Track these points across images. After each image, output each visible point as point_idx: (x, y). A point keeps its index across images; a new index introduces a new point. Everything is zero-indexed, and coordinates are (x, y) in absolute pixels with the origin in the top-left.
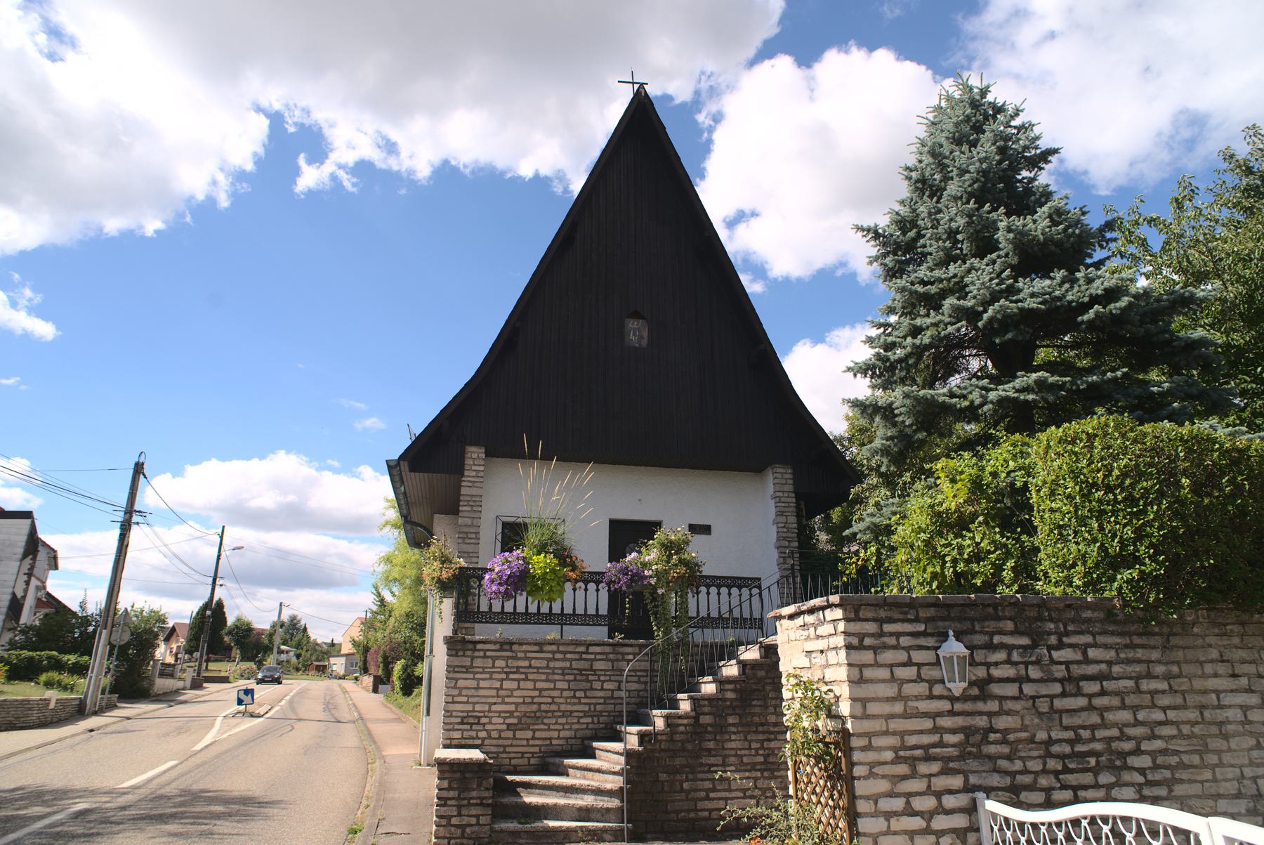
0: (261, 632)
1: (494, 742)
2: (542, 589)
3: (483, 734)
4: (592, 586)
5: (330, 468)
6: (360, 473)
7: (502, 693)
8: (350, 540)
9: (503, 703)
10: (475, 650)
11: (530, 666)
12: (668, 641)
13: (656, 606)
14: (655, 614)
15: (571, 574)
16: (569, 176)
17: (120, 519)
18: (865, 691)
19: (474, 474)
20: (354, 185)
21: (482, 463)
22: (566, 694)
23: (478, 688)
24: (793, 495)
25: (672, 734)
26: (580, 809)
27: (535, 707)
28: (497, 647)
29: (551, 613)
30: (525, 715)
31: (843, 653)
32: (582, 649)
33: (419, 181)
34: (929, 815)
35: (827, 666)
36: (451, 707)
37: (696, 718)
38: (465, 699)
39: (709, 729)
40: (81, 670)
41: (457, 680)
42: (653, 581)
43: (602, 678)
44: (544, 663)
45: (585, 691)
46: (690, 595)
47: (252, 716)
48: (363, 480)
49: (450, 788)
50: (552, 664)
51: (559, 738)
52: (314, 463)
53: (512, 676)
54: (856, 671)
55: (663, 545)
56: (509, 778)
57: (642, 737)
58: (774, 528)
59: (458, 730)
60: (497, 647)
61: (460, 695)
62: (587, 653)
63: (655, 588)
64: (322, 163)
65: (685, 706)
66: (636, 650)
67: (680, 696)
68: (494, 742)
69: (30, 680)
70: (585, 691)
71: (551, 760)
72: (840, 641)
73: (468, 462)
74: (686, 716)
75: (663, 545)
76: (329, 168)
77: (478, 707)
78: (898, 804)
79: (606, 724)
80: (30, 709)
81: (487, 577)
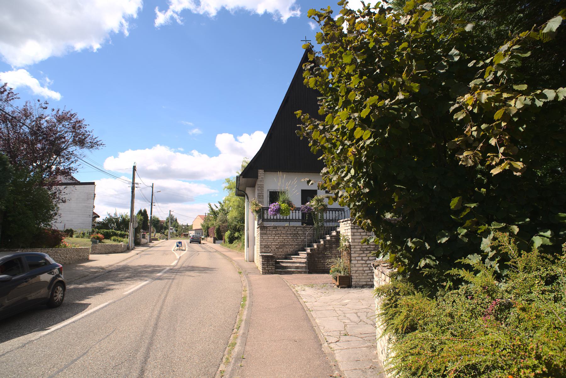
0: (162, 222)
1: (273, 252)
2: (284, 213)
3: (270, 250)
4: (297, 211)
5: (179, 152)
6: (193, 154)
7: (274, 240)
8: (190, 182)
9: (275, 242)
10: (267, 229)
11: (281, 233)
12: (318, 226)
13: (315, 217)
14: (315, 219)
15: (292, 209)
16: (281, 13)
17: (131, 186)
18: (354, 237)
19: (261, 178)
20: (182, 21)
21: (263, 174)
22: (291, 240)
23: (268, 238)
25: (319, 249)
26: (296, 267)
27: (283, 243)
28: (273, 228)
29: (286, 219)
30: (281, 245)
31: (350, 230)
32: (295, 228)
33: (211, 18)
34: (366, 261)
35: (348, 232)
36: (262, 243)
37: (325, 245)
38: (265, 241)
40: (123, 236)
41: (263, 236)
42: (314, 210)
44: (285, 232)
45: (296, 239)
46: (324, 213)
47: (182, 250)
48: (194, 156)
49: (265, 261)
50: (287, 232)
51: (290, 251)
52: (172, 149)
53: (277, 235)
54: (353, 233)
55: (317, 200)
56: (277, 260)
57: (311, 250)
60: (273, 228)
61: (264, 240)
62: (296, 229)
63: (314, 212)
64: (166, 11)
65: (322, 242)
66: (310, 228)
67: (321, 240)
68: (273, 252)
69: (109, 239)
70: (296, 239)
71: (288, 256)
72: (350, 227)
73: (259, 174)
74: (322, 245)
75: (317, 200)
76: (169, 13)
77: (268, 243)
78: (360, 258)
80: (119, 247)
81: (269, 210)
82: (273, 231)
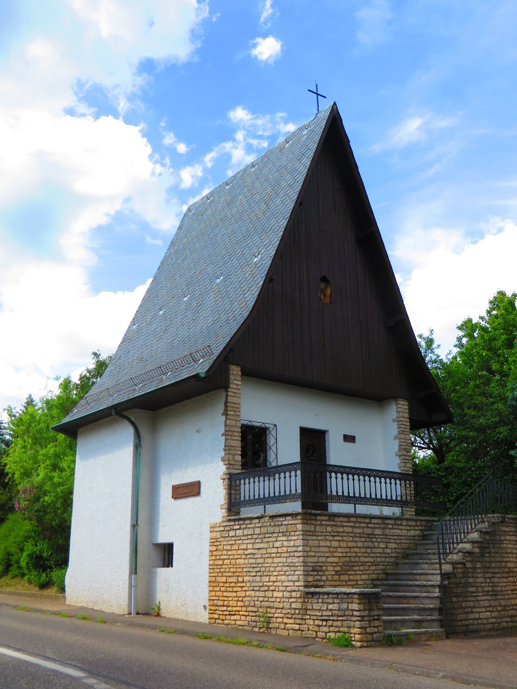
10: (316, 520)
24: (408, 420)
39: (470, 570)
41: (308, 540)
43: (379, 540)
44: (350, 530)
49: (365, 610)
58: (397, 442)
59: (311, 575)
77: (321, 560)
79: (382, 570)
82: (328, 525)
